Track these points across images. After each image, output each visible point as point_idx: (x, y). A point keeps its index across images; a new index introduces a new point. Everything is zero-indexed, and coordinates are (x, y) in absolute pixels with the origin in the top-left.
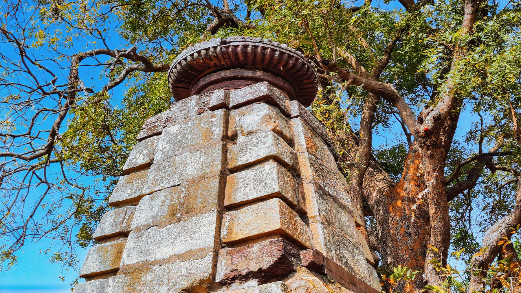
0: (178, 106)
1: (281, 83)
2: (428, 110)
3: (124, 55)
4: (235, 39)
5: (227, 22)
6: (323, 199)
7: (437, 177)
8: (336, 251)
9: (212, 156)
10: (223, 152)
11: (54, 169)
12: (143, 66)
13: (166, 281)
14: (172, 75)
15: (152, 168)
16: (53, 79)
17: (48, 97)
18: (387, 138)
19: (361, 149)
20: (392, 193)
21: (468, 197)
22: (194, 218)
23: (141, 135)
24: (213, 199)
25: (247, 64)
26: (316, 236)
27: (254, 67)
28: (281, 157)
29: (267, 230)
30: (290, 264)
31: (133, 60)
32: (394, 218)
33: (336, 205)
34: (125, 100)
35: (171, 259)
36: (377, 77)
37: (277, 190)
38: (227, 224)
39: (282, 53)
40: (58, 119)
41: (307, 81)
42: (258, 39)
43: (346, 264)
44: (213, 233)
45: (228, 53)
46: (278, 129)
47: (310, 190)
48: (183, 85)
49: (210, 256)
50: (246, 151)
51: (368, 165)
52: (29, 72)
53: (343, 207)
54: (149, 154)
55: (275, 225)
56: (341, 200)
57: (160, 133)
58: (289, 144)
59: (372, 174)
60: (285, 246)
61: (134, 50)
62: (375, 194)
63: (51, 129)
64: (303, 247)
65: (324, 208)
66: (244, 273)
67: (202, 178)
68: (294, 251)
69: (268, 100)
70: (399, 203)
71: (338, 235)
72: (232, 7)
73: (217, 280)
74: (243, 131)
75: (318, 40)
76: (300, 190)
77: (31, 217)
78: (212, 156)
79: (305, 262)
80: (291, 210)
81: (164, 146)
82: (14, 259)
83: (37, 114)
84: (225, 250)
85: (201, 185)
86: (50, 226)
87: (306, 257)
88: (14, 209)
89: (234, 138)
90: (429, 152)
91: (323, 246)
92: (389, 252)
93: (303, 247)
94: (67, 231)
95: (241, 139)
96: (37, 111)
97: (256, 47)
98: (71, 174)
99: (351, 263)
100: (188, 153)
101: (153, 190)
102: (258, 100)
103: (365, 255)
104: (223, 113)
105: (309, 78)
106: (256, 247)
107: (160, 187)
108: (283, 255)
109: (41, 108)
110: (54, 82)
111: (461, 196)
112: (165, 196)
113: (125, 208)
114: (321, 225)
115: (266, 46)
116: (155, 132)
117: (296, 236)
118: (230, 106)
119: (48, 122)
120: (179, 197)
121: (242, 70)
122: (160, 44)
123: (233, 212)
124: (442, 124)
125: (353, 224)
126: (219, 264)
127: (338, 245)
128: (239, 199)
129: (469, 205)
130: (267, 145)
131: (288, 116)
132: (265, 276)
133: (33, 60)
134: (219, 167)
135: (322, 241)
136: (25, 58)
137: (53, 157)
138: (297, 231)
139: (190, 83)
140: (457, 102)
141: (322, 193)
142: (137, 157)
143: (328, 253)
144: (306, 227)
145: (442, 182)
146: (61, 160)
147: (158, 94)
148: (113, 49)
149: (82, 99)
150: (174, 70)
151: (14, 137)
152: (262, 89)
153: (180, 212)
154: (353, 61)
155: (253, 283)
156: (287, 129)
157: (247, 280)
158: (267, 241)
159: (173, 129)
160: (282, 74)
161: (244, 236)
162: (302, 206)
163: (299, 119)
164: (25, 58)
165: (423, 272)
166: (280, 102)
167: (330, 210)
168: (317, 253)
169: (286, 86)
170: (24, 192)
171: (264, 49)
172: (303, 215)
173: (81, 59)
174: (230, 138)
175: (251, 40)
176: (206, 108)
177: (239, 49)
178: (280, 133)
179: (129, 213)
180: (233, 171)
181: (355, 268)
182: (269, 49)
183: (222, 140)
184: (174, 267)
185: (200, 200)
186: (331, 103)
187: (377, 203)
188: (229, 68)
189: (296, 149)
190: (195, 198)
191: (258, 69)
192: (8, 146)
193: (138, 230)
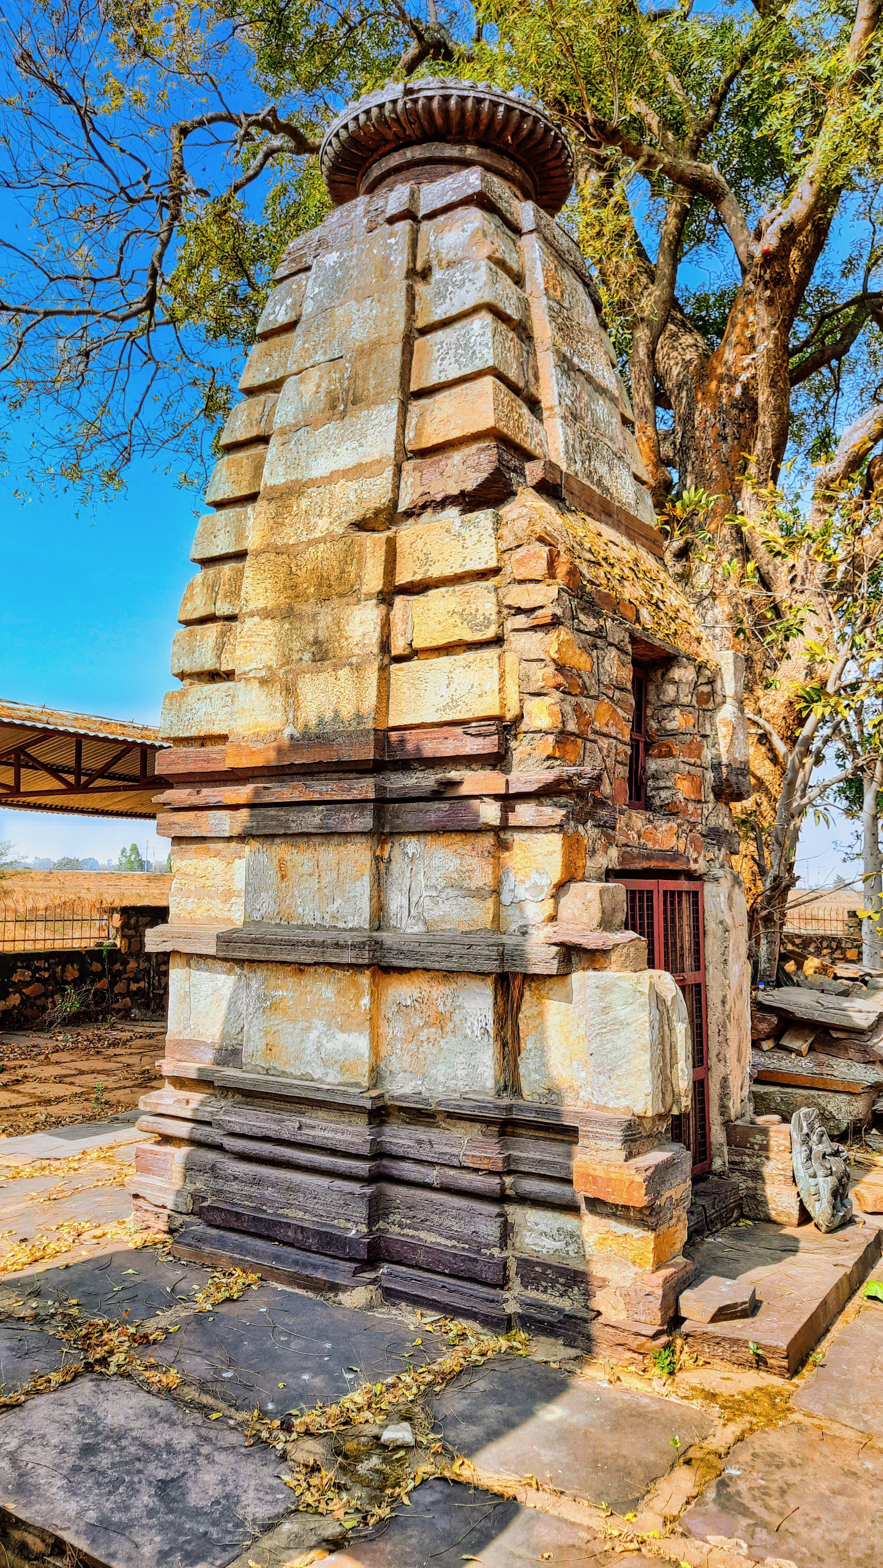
0: (335, 217)
1: (507, 167)
2: (774, 213)
3: (255, 123)
4: (429, 81)
5: (436, 49)
6: (569, 377)
7: (776, 337)
8: (583, 463)
9: (391, 306)
10: (407, 299)
11: (162, 337)
12: (292, 144)
13: (326, 511)
14: (325, 158)
15: (299, 329)
16: (145, 173)
17: (136, 207)
18: (708, 272)
19: (657, 291)
20: (703, 371)
21: (837, 376)
22: (365, 413)
23: (281, 272)
24: (393, 381)
25: (449, 132)
26: (552, 440)
27: (461, 140)
28: (501, 305)
29: (474, 430)
30: (508, 484)
31: (273, 132)
32: (704, 410)
33: (590, 388)
34: (266, 208)
35: (331, 478)
36: (694, 153)
37: (491, 363)
38: (414, 422)
39: (509, 109)
40: (158, 248)
41: (552, 164)
42: (467, 83)
43: (599, 483)
44: (393, 437)
45: (416, 111)
46: (497, 255)
47: (547, 362)
48: (346, 177)
49: (389, 472)
50: (445, 297)
51: (668, 319)
52: (101, 160)
53: (602, 391)
54: (294, 304)
55: (487, 421)
56: (599, 380)
57: (308, 269)
58: (517, 283)
59: (674, 336)
60: (500, 455)
61: (273, 112)
62: (675, 371)
63: (148, 266)
64: (530, 457)
65: (569, 392)
66: (439, 498)
67: (376, 345)
68: (515, 462)
69: (482, 201)
70: (714, 385)
71: (589, 438)
72: (444, 17)
73: (401, 509)
74: (440, 261)
75: (591, 82)
76: (531, 363)
77: (137, 415)
78: (391, 306)
79: (532, 480)
80: (513, 396)
81: (317, 290)
82: (121, 482)
83: (127, 238)
84: (412, 463)
85: (374, 357)
86: (168, 432)
87: (534, 471)
88: (111, 403)
89: (425, 274)
90: (768, 293)
91: (562, 455)
92: (690, 468)
93: (530, 457)
94: (195, 438)
95: (437, 275)
96: (125, 234)
97: (464, 99)
98: (192, 345)
99: (607, 482)
100: (353, 302)
101: (302, 367)
102: (466, 202)
103: (633, 469)
104: (408, 228)
105: (558, 157)
106: (456, 456)
107: (311, 362)
108: (497, 469)
109: (131, 228)
110: (146, 178)
111: (824, 370)
112: (321, 377)
113: (262, 398)
114: (560, 421)
115: (481, 95)
116: (302, 265)
117: (519, 439)
118: (420, 215)
119: (143, 252)
120: (341, 379)
121: (441, 145)
122: (322, 97)
123: (423, 402)
124: (793, 242)
125: (616, 420)
126: (402, 485)
127: (589, 453)
128: (433, 379)
129: (837, 389)
130: (478, 285)
131: (517, 231)
132: (469, 502)
133: (107, 138)
134: (402, 326)
135: (561, 447)
136: (91, 133)
137: (160, 315)
138: (521, 431)
139: (356, 174)
140: (827, 198)
141: (568, 367)
142: (276, 313)
143: (569, 466)
144: (537, 424)
145: (784, 351)
146: (173, 321)
147: (318, 196)
148: (237, 111)
149: (196, 209)
150: (328, 149)
151: (95, 281)
152: (472, 180)
153: (343, 403)
154: (653, 120)
155: (452, 512)
156: (514, 255)
157: (443, 508)
158: (474, 447)
159: (331, 258)
160: (510, 150)
161: (440, 440)
162: (533, 390)
163: (534, 235)
164: (91, 133)
165: (739, 498)
166: (502, 205)
167: (579, 397)
168: (551, 466)
169: (517, 173)
170: (123, 374)
171: (479, 101)
172: (534, 405)
173: (184, 132)
174: (419, 274)
175: (464, 83)
176: (380, 220)
177: (435, 104)
178: (501, 264)
179: (269, 405)
180: (424, 331)
181: (613, 490)
182: (487, 103)
183: (407, 278)
184: (338, 488)
185: (372, 382)
186: (605, 206)
187: (680, 387)
188: (419, 142)
189: (528, 291)
190: (365, 379)
191: (469, 143)
192: (88, 297)
193: (283, 432)
